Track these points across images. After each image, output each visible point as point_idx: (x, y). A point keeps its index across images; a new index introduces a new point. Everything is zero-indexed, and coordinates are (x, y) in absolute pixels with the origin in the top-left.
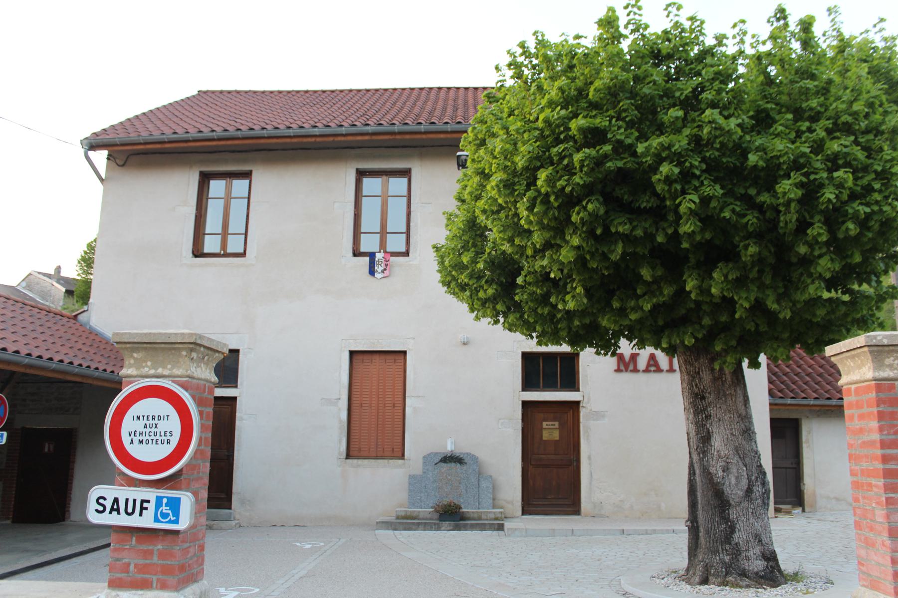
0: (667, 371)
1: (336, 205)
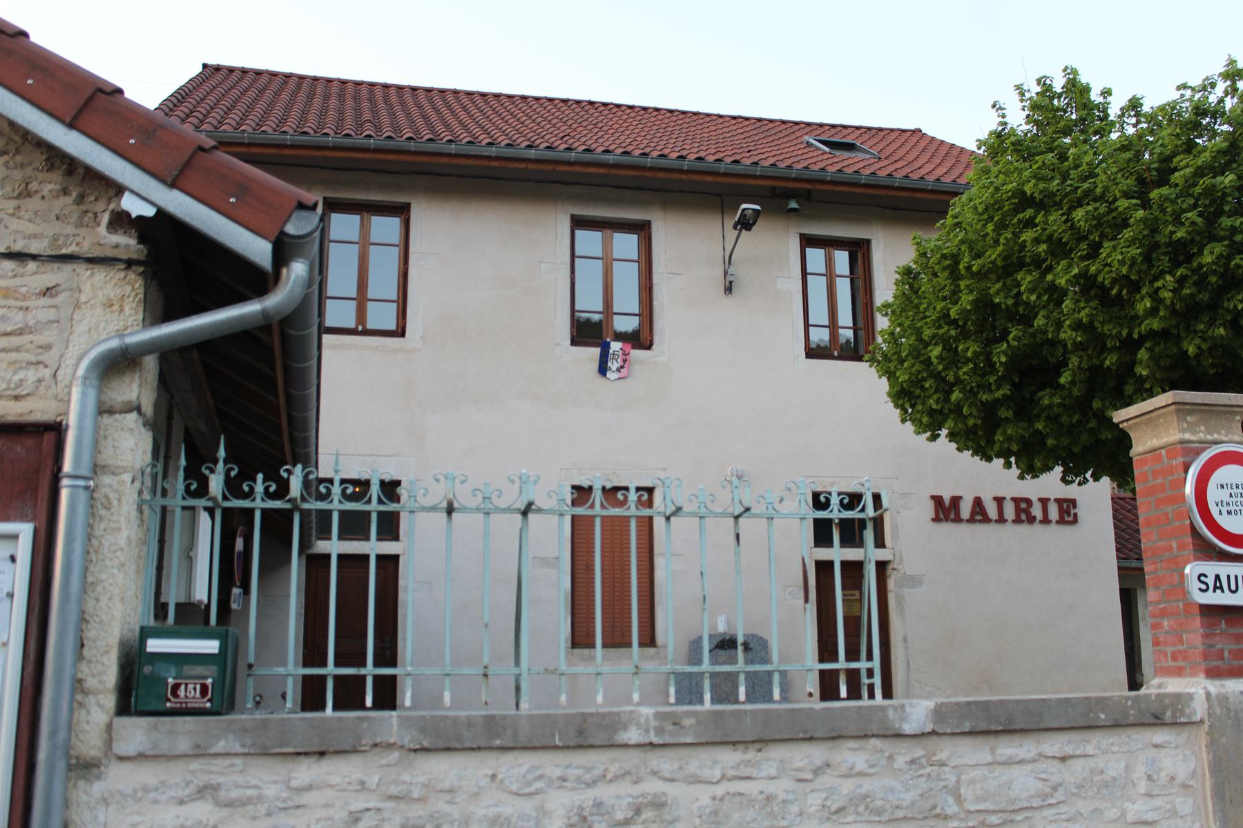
0: (996, 521)
1: (544, 266)
